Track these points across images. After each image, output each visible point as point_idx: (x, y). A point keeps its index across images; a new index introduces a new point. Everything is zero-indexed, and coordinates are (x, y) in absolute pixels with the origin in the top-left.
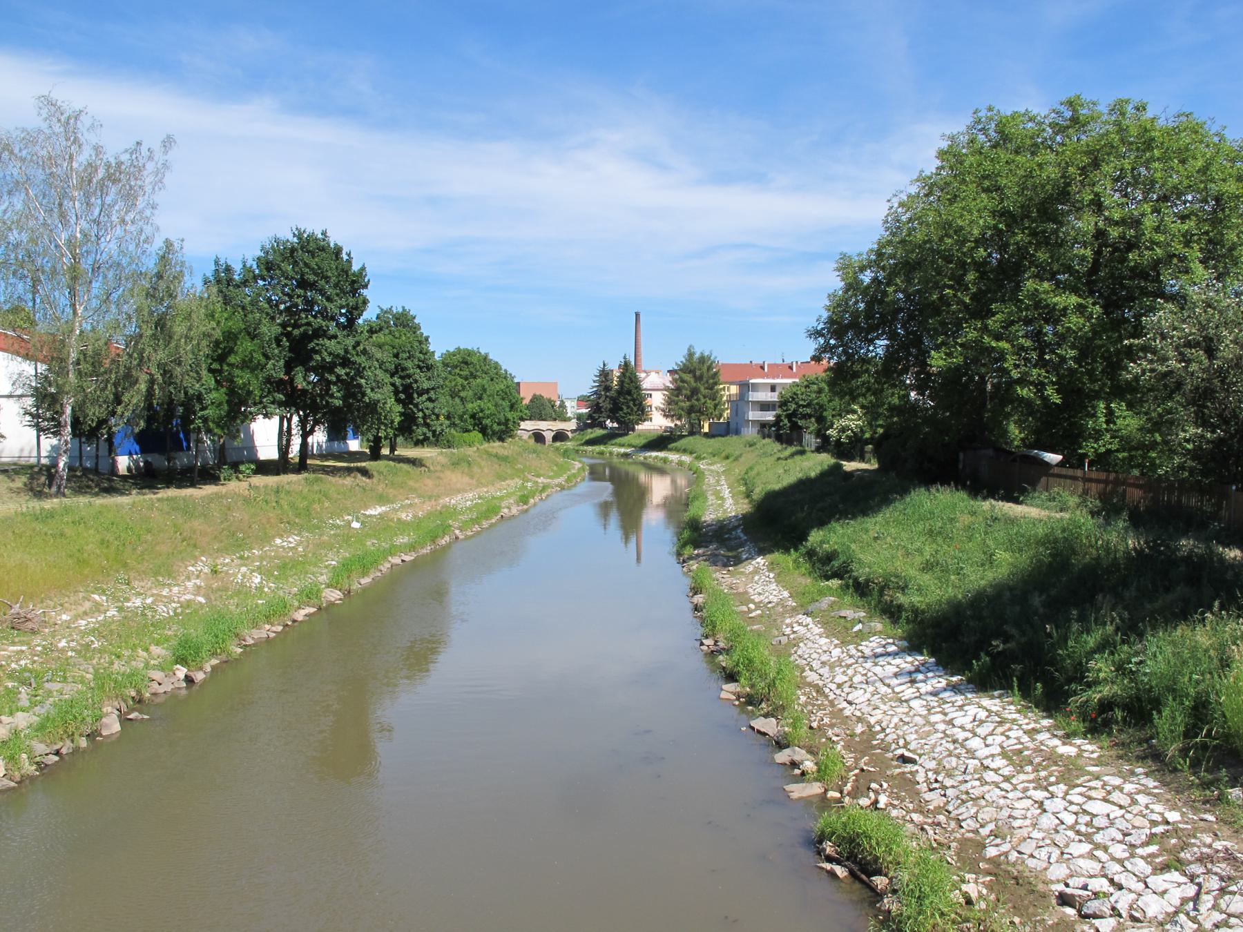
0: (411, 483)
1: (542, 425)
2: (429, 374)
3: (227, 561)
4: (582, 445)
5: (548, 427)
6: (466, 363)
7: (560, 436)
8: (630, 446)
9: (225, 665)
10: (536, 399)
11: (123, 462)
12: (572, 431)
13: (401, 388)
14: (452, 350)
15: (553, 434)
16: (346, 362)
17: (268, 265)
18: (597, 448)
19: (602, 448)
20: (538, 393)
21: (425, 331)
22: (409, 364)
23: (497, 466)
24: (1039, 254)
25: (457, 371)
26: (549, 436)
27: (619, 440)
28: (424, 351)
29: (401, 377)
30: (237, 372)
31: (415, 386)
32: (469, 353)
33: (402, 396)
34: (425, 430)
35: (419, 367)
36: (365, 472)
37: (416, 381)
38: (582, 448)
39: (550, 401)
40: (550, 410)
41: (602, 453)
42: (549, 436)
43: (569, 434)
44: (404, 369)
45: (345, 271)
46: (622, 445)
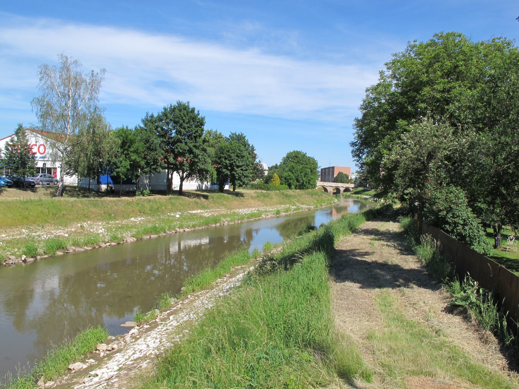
0: (225, 202)
1: (339, 185)
2: (242, 159)
3: (100, 223)
4: (352, 194)
5: (342, 186)
6: (297, 157)
7: (347, 190)
8: (370, 195)
9: (50, 258)
10: (340, 174)
11: (104, 187)
12: (353, 188)
13: (229, 165)
14: (292, 151)
15: (344, 189)
16: (190, 151)
17: (165, 114)
18: (357, 195)
19: (359, 196)
20: (341, 171)
21: (251, 143)
22: (232, 155)
23: (282, 199)
24: (409, 107)
25: (293, 160)
26: (342, 189)
27: (366, 193)
28: (241, 150)
29: (229, 160)
30: (132, 154)
31: (234, 164)
32: (298, 153)
33: (230, 168)
34: (240, 182)
35: (237, 156)
36: (206, 197)
37: (235, 162)
38: (352, 195)
39: (346, 175)
40: (345, 179)
41: (358, 198)
42: (330, 190)
43: (351, 189)
44: (231, 157)
45: (194, 119)
46: (367, 195)
